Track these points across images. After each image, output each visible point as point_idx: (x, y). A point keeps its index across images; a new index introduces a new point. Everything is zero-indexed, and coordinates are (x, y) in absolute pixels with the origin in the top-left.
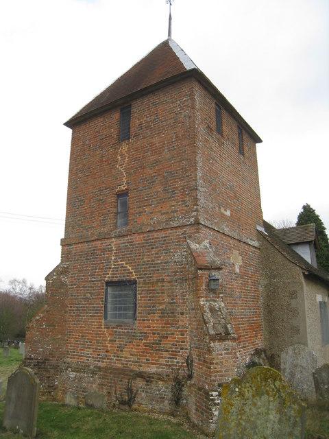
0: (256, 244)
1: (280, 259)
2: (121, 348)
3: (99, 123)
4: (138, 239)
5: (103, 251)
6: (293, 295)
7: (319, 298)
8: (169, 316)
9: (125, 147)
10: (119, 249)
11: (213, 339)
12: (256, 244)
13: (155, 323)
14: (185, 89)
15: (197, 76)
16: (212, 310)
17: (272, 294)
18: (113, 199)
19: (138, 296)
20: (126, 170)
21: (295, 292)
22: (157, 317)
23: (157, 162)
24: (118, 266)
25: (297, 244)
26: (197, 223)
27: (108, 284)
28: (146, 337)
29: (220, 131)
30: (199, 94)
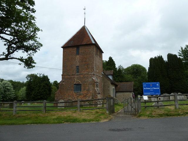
0: (101, 76)
1: (106, 80)
2: (78, 97)
3: (71, 49)
4: (82, 76)
5: (73, 78)
6: (108, 87)
7: (113, 88)
8: (88, 90)
9: (78, 56)
10: (77, 78)
11: (98, 94)
12: (101, 76)
13: (85, 92)
14: (92, 47)
15: (96, 45)
16: (97, 89)
17: (104, 86)
18: (75, 67)
19: (82, 87)
20: (78, 61)
21: (109, 86)
22: (86, 91)
23: (85, 61)
24: (76, 81)
25: (109, 75)
26: (94, 74)
27: (75, 84)
28: (83, 94)
29: (97, 54)
30: (95, 49)
